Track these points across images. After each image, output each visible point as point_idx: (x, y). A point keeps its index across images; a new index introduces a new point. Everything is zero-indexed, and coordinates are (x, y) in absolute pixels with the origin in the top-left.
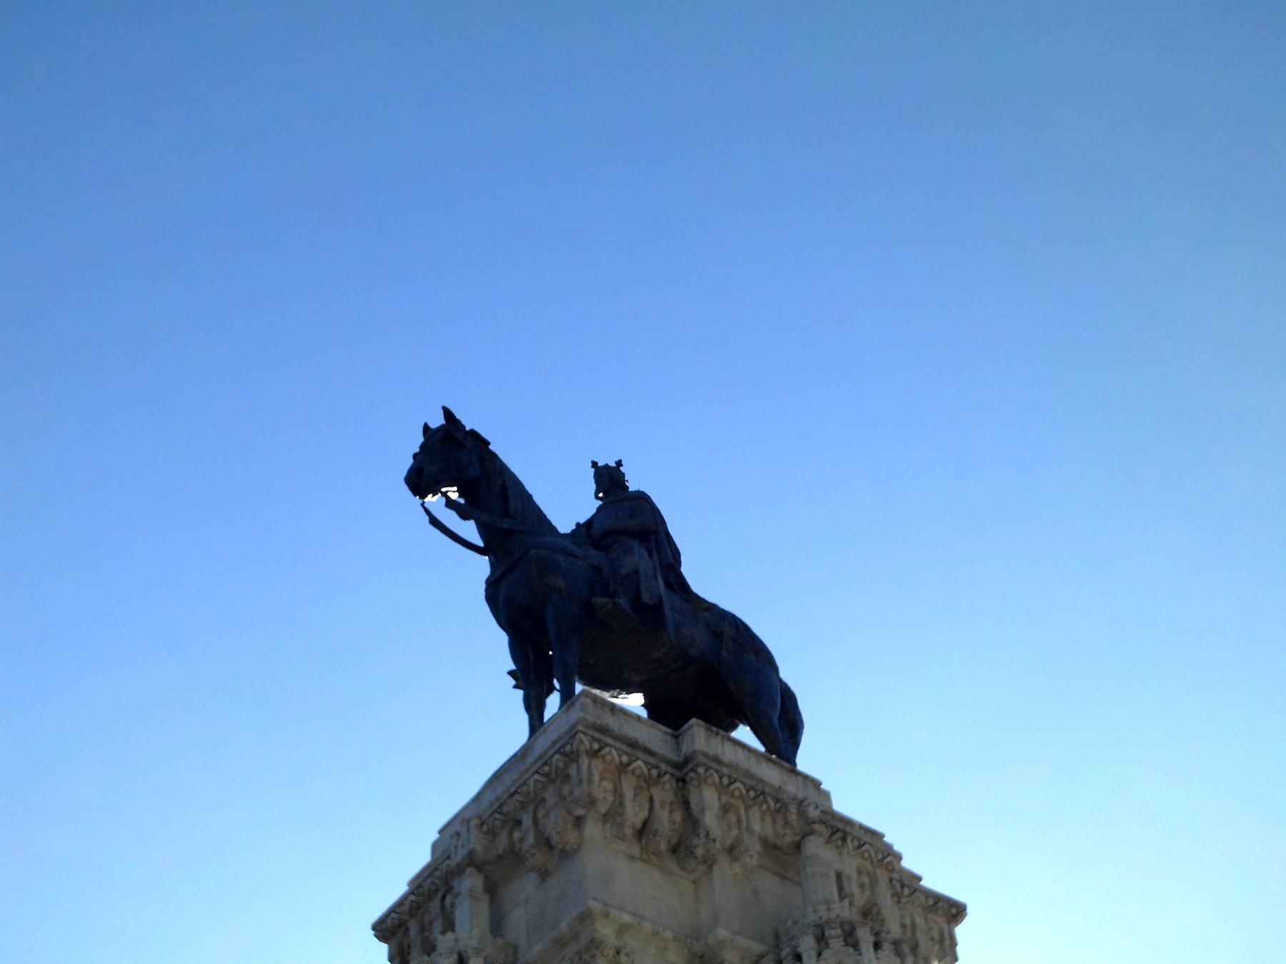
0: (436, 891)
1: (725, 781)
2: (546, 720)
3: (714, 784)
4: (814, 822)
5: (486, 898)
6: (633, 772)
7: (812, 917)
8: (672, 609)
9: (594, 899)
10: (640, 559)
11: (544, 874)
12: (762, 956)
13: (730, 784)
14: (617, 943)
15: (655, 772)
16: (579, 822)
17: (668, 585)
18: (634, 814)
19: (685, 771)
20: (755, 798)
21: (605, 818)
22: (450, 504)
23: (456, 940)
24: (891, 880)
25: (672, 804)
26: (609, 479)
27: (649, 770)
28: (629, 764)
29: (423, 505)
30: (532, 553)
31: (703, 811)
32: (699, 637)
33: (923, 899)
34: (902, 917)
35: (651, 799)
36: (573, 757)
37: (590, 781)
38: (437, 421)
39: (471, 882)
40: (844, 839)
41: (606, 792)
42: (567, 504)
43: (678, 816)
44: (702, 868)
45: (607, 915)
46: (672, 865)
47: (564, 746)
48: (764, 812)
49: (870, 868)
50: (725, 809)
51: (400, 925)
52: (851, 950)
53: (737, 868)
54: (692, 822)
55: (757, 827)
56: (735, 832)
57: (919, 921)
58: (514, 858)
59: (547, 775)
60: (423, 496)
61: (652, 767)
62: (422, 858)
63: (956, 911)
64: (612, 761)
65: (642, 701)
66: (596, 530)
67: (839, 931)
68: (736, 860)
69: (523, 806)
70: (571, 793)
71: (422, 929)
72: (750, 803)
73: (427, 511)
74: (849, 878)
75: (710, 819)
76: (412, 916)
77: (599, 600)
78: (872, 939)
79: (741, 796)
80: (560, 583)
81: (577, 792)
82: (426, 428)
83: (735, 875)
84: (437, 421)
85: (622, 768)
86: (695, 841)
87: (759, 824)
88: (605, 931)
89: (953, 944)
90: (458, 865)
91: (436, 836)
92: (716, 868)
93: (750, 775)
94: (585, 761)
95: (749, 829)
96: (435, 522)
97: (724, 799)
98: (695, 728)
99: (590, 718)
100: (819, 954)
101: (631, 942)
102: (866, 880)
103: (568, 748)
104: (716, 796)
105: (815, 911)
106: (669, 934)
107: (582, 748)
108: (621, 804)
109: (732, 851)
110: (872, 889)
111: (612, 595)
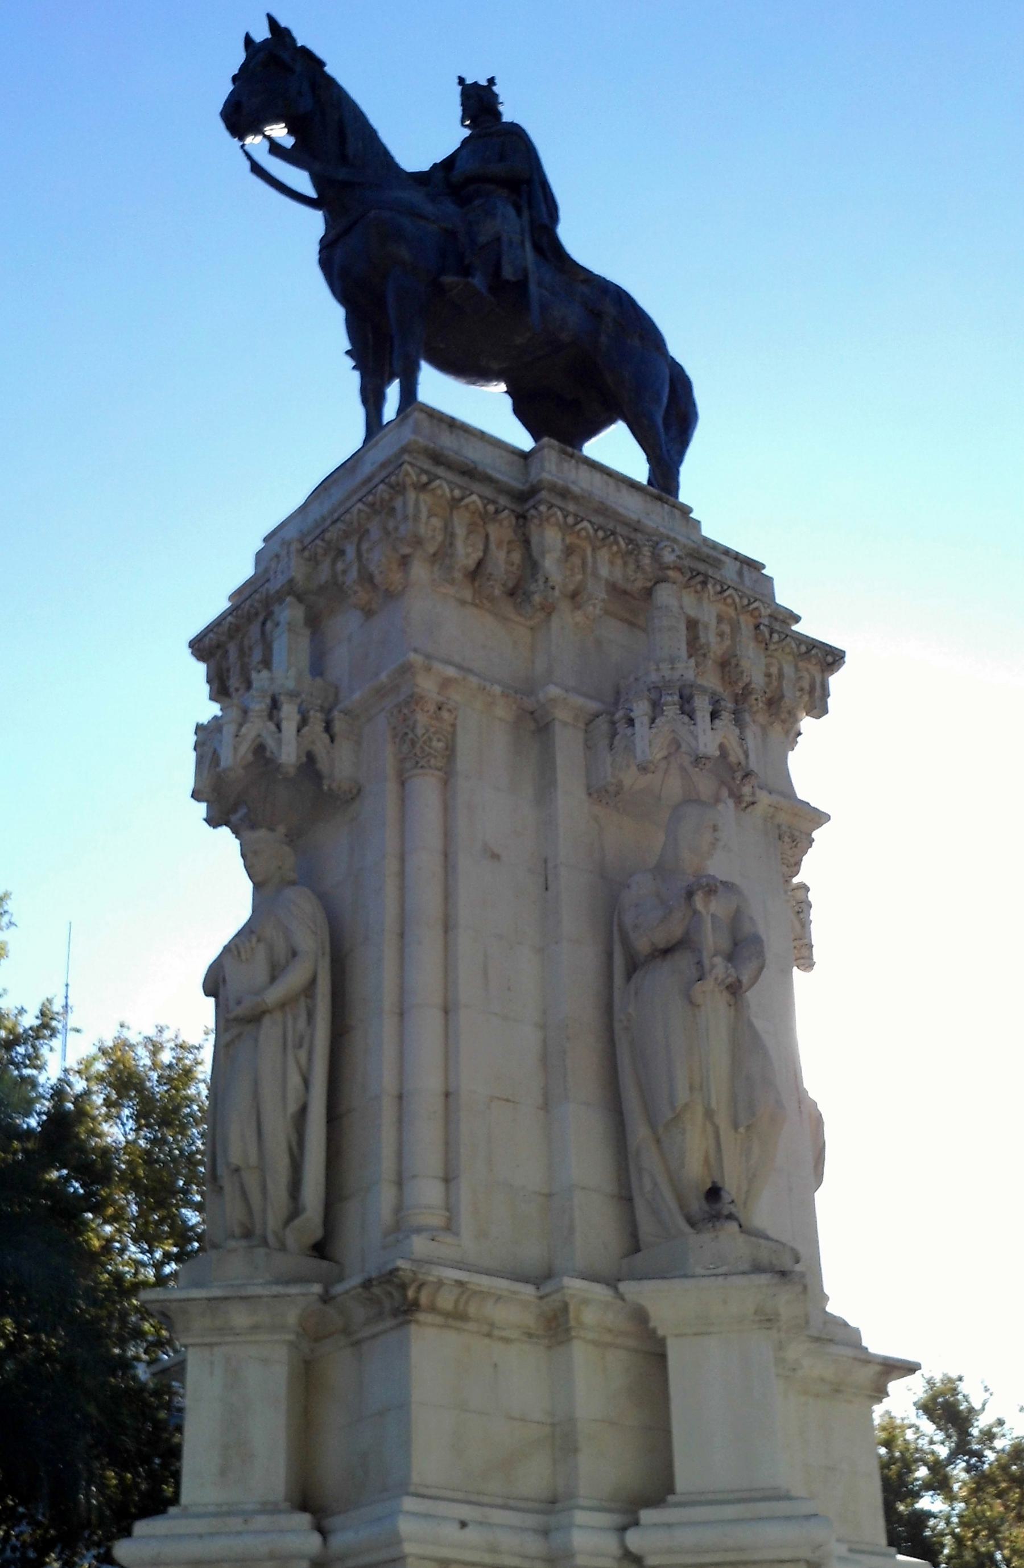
0: (257, 614)
1: (570, 520)
2: (385, 422)
3: (558, 524)
4: (668, 568)
5: (307, 632)
6: (467, 506)
7: (654, 677)
8: (540, 284)
9: (415, 650)
10: (506, 222)
11: (369, 613)
12: (597, 716)
13: (576, 524)
14: (440, 699)
15: (491, 508)
16: (405, 561)
17: (538, 248)
18: (466, 554)
19: (527, 507)
20: (603, 539)
21: (435, 558)
22: (275, 148)
23: (272, 680)
24: (757, 627)
25: (509, 543)
26: (479, 102)
27: (485, 506)
28: (462, 499)
29: (243, 146)
30: (373, 213)
31: (543, 554)
32: (570, 316)
33: (794, 645)
34: (768, 666)
35: (487, 536)
36: (399, 489)
37: (416, 518)
38: (262, 33)
39: (290, 613)
40: (704, 583)
41: (434, 530)
42: (421, 135)
43: (517, 557)
44: (541, 615)
45: (428, 669)
46: (507, 608)
47: (388, 476)
48: (614, 555)
49: (733, 613)
50: (569, 551)
51: (218, 646)
52: (686, 719)
53: (579, 617)
54: (531, 564)
55: (604, 572)
56: (579, 577)
57: (788, 670)
58: (335, 591)
59: (372, 505)
60: (242, 138)
61: (487, 501)
62: (246, 571)
63: (832, 658)
64: (443, 495)
65: (505, 389)
66: (456, 176)
67: (676, 698)
68: (578, 607)
69: (347, 535)
70: (396, 529)
71: (242, 653)
72: (598, 544)
73: (247, 155)
74: (706, 627)
75: (550, 563)
76: (231, 637)
77: (448, 279)
78: (710, 708)
79: (588, 537)
80: (404, 253)
81: (402, 528)
82: (248, 41)
83: (577, 624)
84: (262, 33)
85: (455, 503)
86: (533, 587)
87: (606, 567)
88: (427, 685)
89: (825, 693)
90: (277, 592)
91: (260, 545)
92: (555, 618)
93: (603, 510)
94: (411, 495)
95: (595, 575)
96: (257, 169)
97: (568, 540)
98: (546, 451)
99: (422, 441)
100: (653, 721)
101: (456, 696)
102: (726, 628)
103: (393, 478)
104: (559, 536)
105: (658, 670)
106: (497, 689)
107: (408, 481)
108: (451, 544)
109: (574, 596)
110: (733, 639)
111: (466, 271)
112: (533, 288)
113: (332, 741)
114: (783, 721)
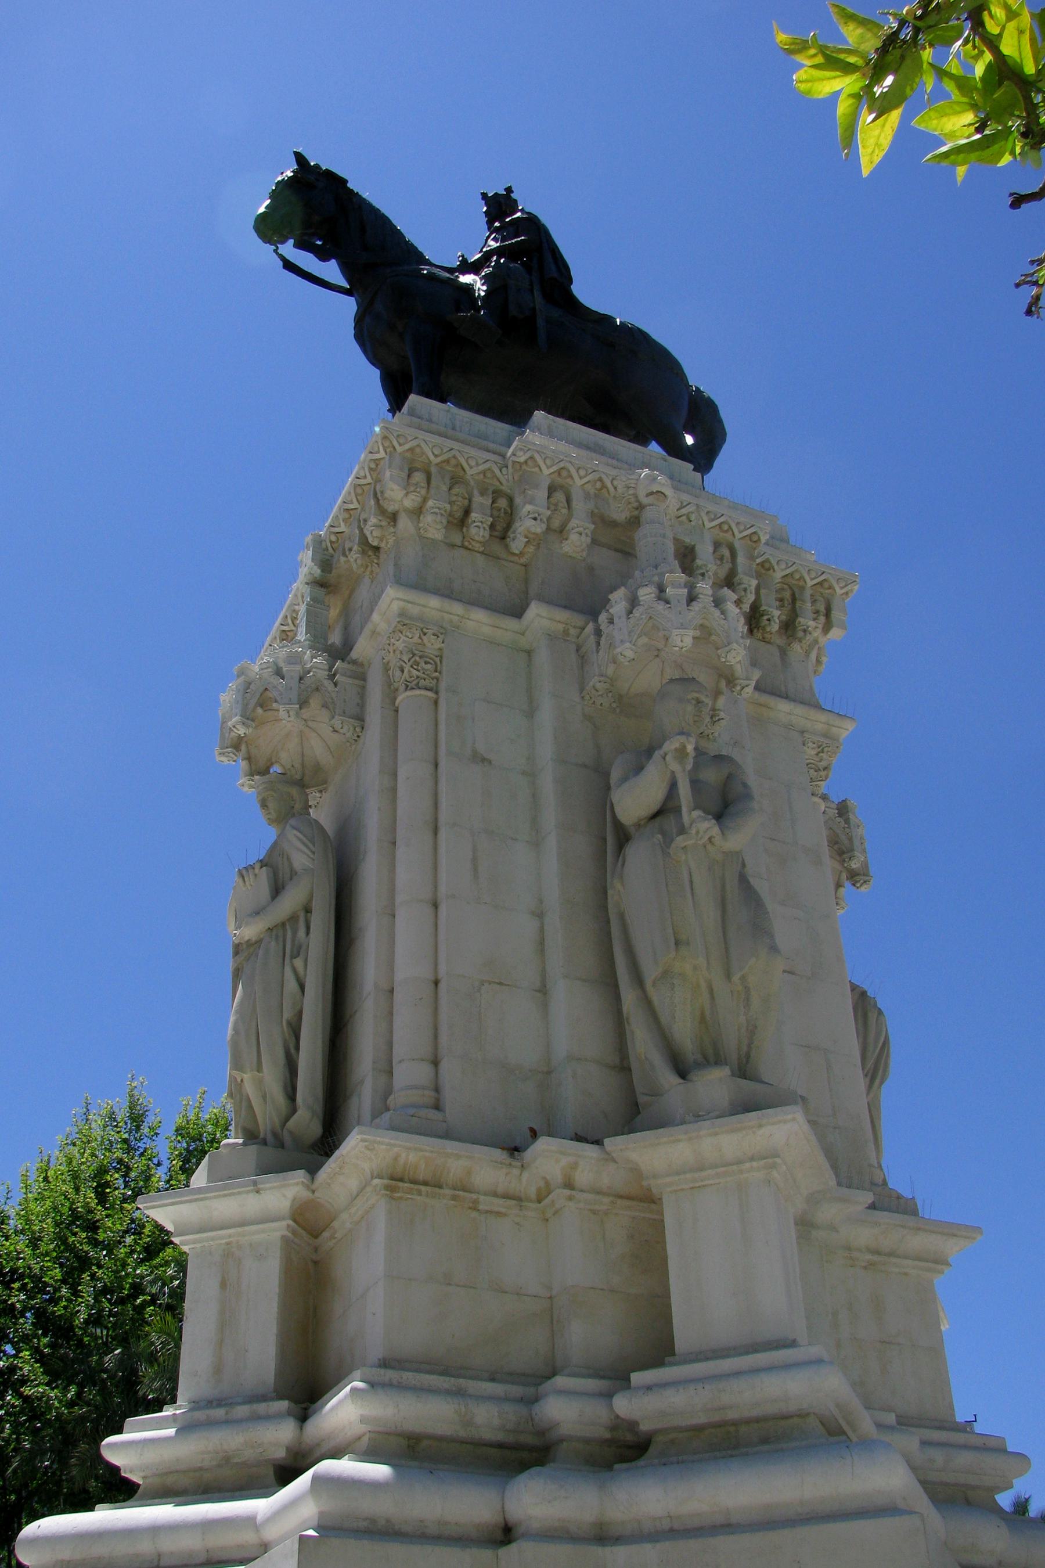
42: (450, 238)
112: (540, 322)
113: (616, 1162)
114: (800, 641)
